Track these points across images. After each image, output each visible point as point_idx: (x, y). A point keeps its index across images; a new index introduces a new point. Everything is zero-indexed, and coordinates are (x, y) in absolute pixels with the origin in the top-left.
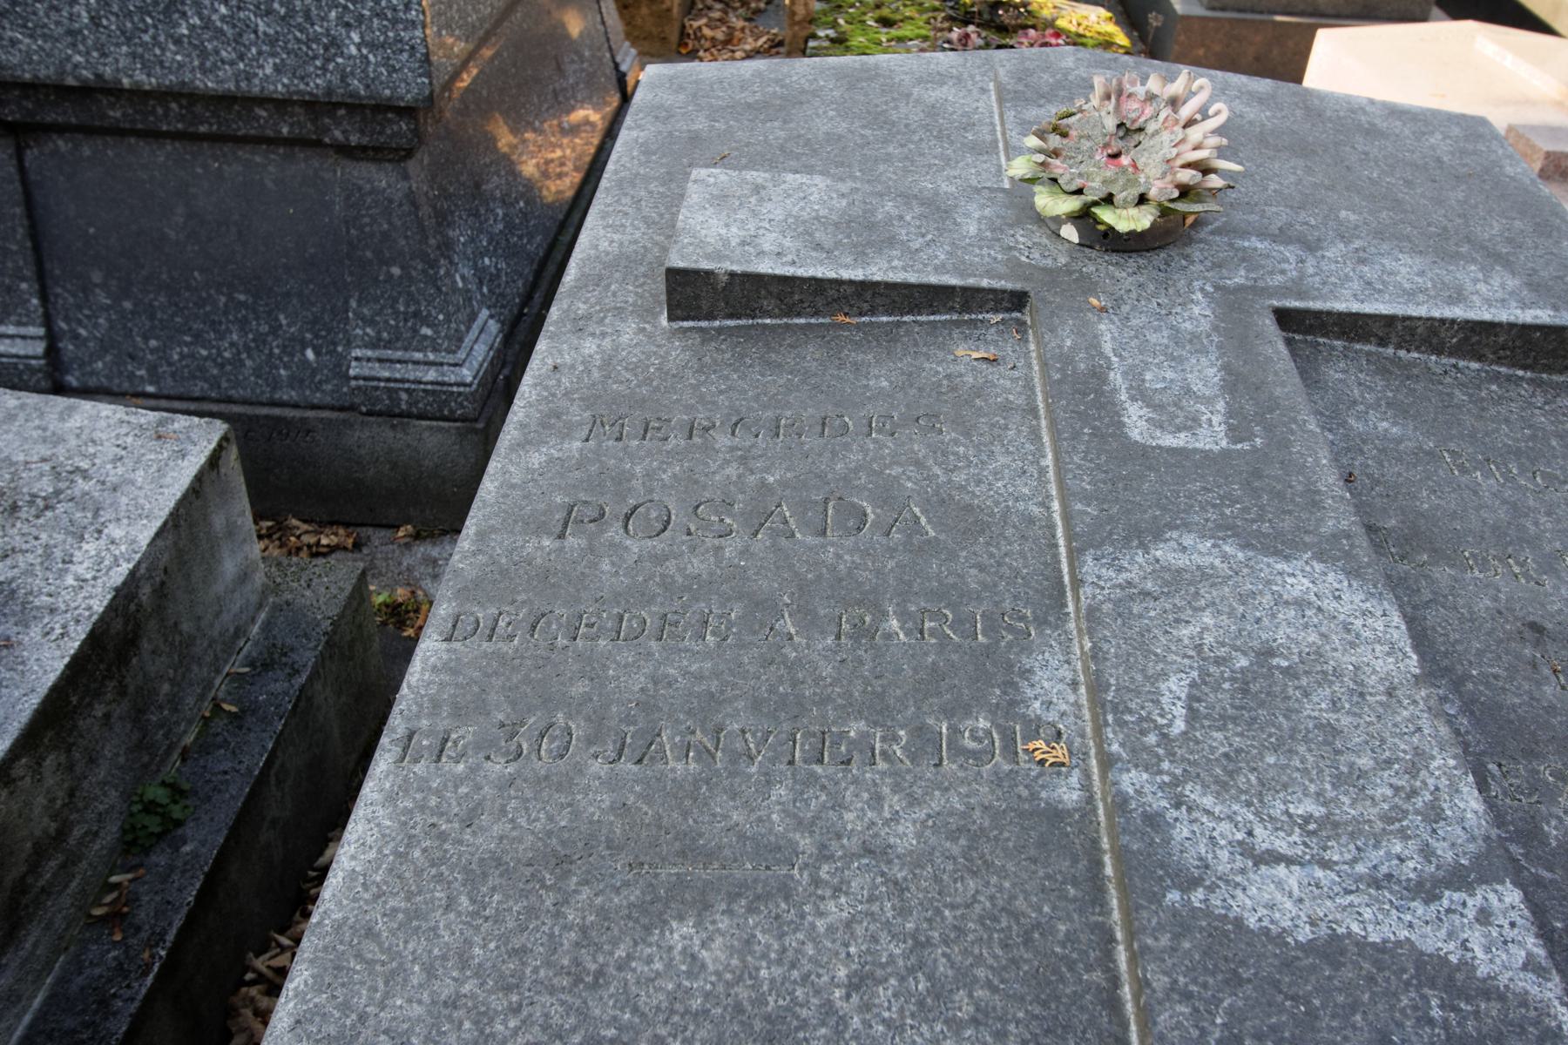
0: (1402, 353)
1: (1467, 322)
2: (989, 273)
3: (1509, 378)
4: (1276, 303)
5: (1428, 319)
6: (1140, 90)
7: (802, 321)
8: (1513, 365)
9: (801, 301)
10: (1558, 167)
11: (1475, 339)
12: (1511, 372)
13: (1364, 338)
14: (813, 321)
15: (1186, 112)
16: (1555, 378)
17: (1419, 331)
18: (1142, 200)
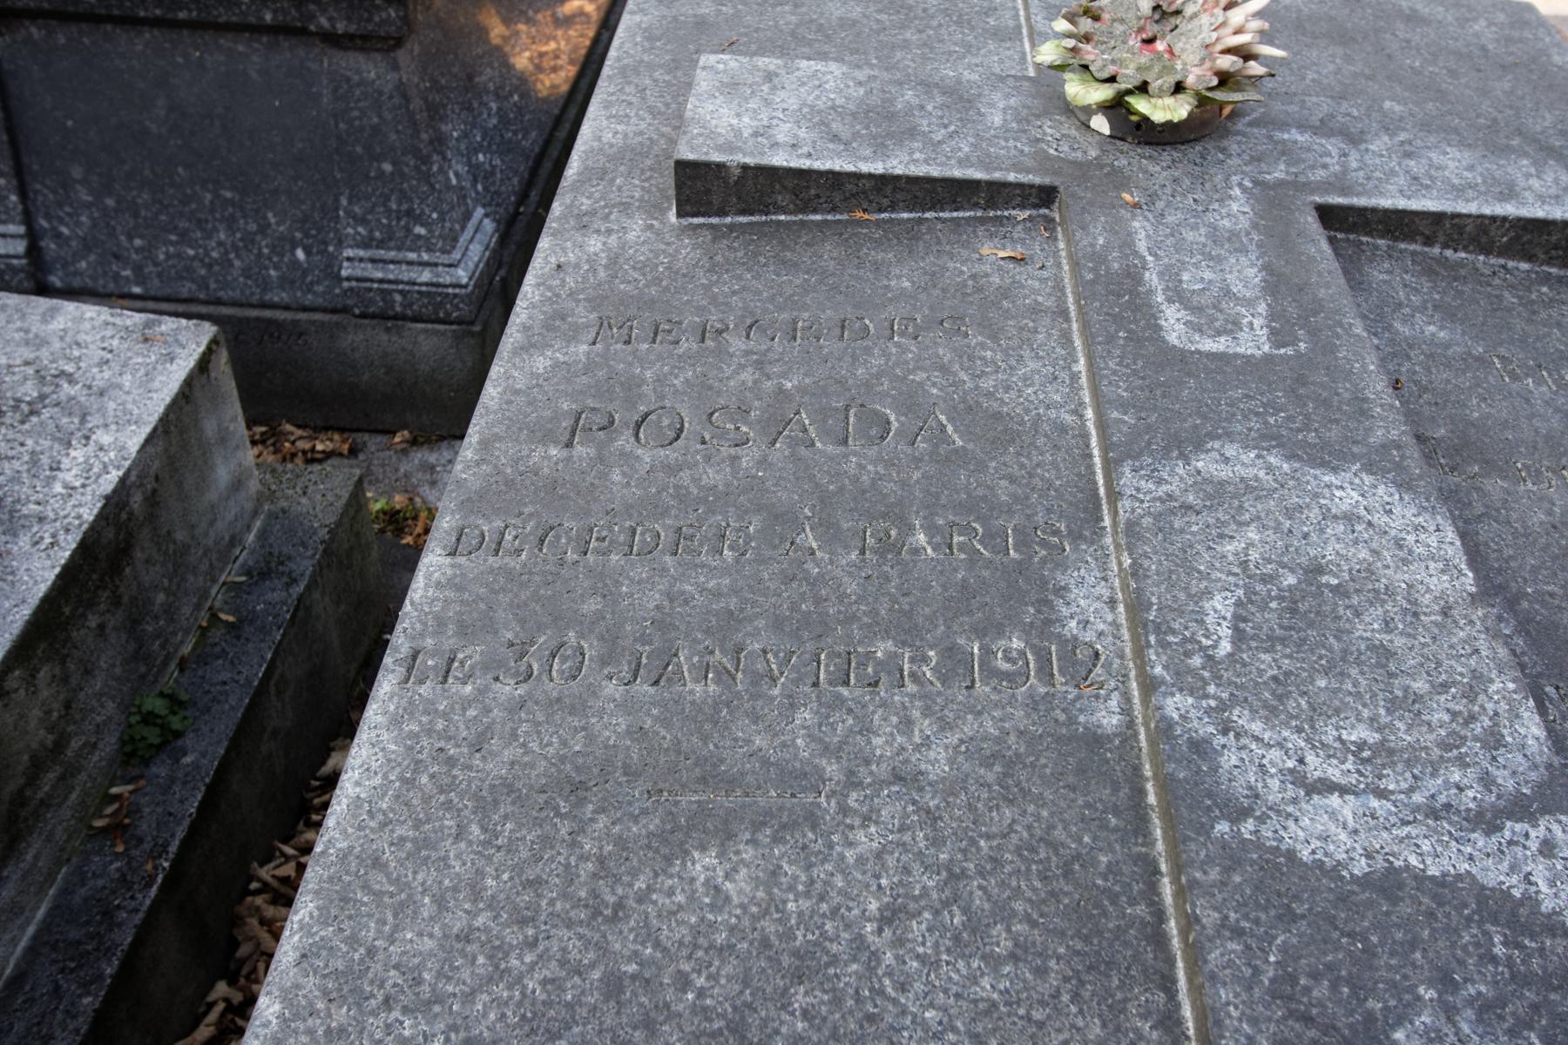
0: (1449, 253)
1: (1519, 219)
2: (1016, 167)
7: (818, 217)
9: (818, 196)
13: (1410, 237)
14: (829, 217)
18: (1179, 88)
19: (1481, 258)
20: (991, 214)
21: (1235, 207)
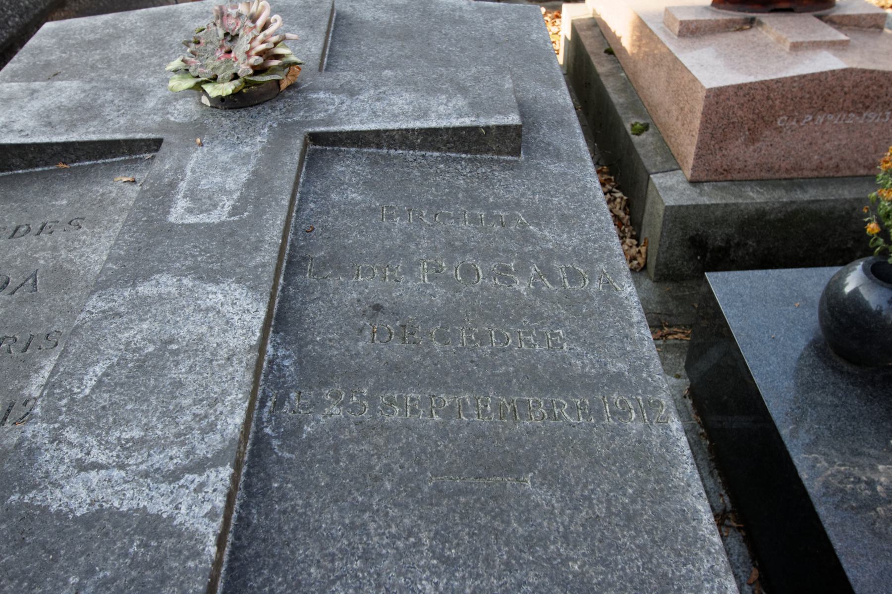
0: (392, 152)
1: (421, 129)
2: (145, 130)
3: (454, 160)
4: (310, 130)
5: (398, 130)
6: (233, 12)
7: (40, 169)
8: (458, 152)
9: (34, 158)
10: (688, 29)
11: (430, 139)
12: (458, 155)
13: (367, 144)
14: (46, 168)
15: (260, 22)
16: (484, 156)
17: (397, 137)
18: (236, 76)
19: (411, 152)
20: (134, 157)
21: (259, 139)
